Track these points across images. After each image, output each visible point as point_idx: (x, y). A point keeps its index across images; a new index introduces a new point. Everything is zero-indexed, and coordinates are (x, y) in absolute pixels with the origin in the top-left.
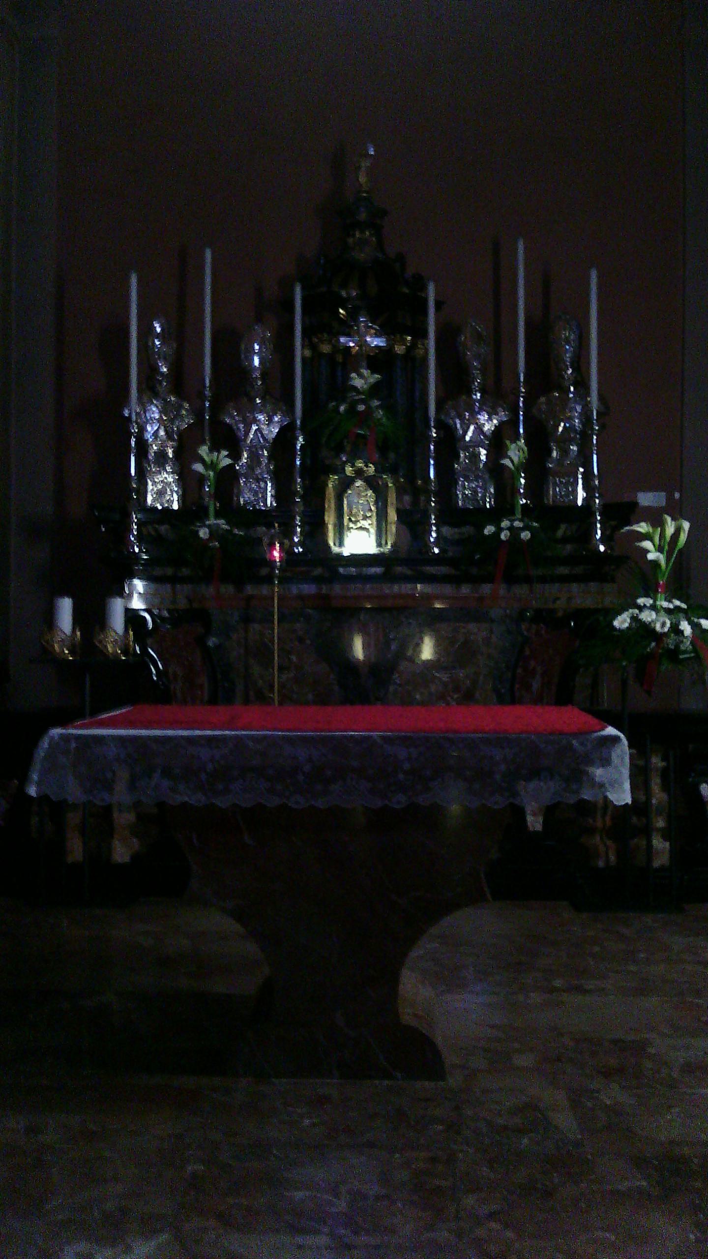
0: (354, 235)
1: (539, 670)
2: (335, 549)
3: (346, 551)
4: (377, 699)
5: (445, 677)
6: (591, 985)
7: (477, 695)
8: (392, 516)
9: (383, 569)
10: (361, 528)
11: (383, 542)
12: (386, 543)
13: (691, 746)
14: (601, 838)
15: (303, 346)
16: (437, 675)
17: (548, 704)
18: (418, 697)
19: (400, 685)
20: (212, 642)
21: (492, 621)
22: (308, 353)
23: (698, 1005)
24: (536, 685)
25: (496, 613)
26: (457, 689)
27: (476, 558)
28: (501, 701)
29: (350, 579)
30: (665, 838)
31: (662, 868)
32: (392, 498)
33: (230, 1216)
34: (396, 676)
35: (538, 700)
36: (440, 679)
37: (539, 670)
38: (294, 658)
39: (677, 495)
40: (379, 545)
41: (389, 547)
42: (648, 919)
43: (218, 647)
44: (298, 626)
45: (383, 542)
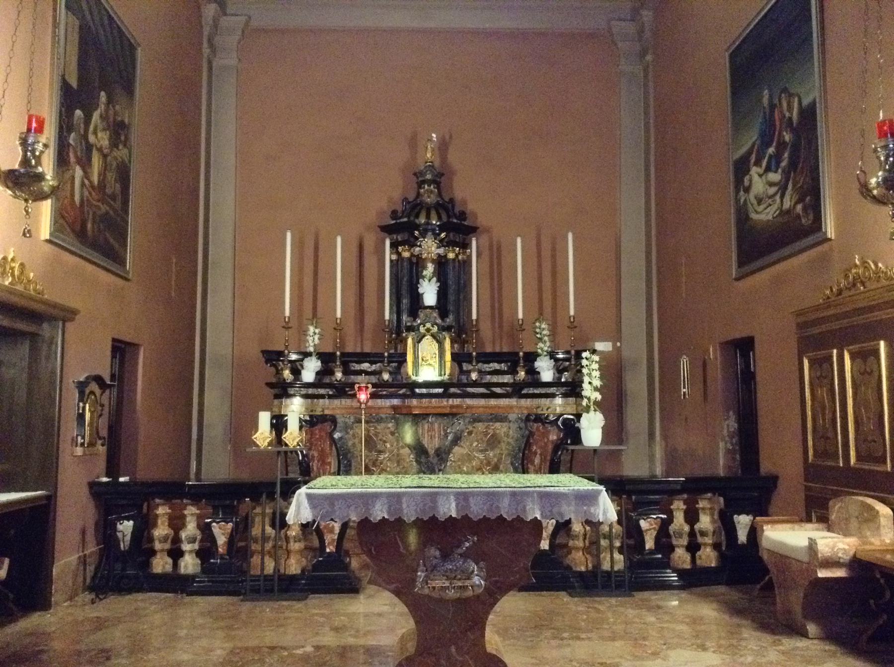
0: (424, 188)
1: (539, 451)
2: (414, 378)
3: (421, 379)
4: (440, 470)
5: (481, 456)
6: (583, 636)
7: (501, 466)
8: (448, 357)
9: (443, 390)
10: (430, 365)
11: (443, 373)
12: (445, 375)
13: (634, 497)
14: (583, 554)
15: (391, 253)
16: (476, 455)
17: (545, 473)
18: (465, 469)
19: (454, 461)
20: (337, 435)
21: (510, 422)
22: (394, 257)
23: (645, 645)
24: (537, 461)
25: (512, 417)
26: (489, 464)
27: (443, 390)
28: (516, 471)
29: (422, 396)
30: (621, 552)
31: (619, 571)
32: (447, 344)
33: (475, 645)
34: (451, 455)
35: (537, 471)
36: (478, 458)
37: (539, 451)
38: (388, 445)
39: (618, 344)
40: (440, 375)
41: (446, 376)
42: (613, 601)
43: (341, 438)
44: (390, 425)
45: (443, 373)
